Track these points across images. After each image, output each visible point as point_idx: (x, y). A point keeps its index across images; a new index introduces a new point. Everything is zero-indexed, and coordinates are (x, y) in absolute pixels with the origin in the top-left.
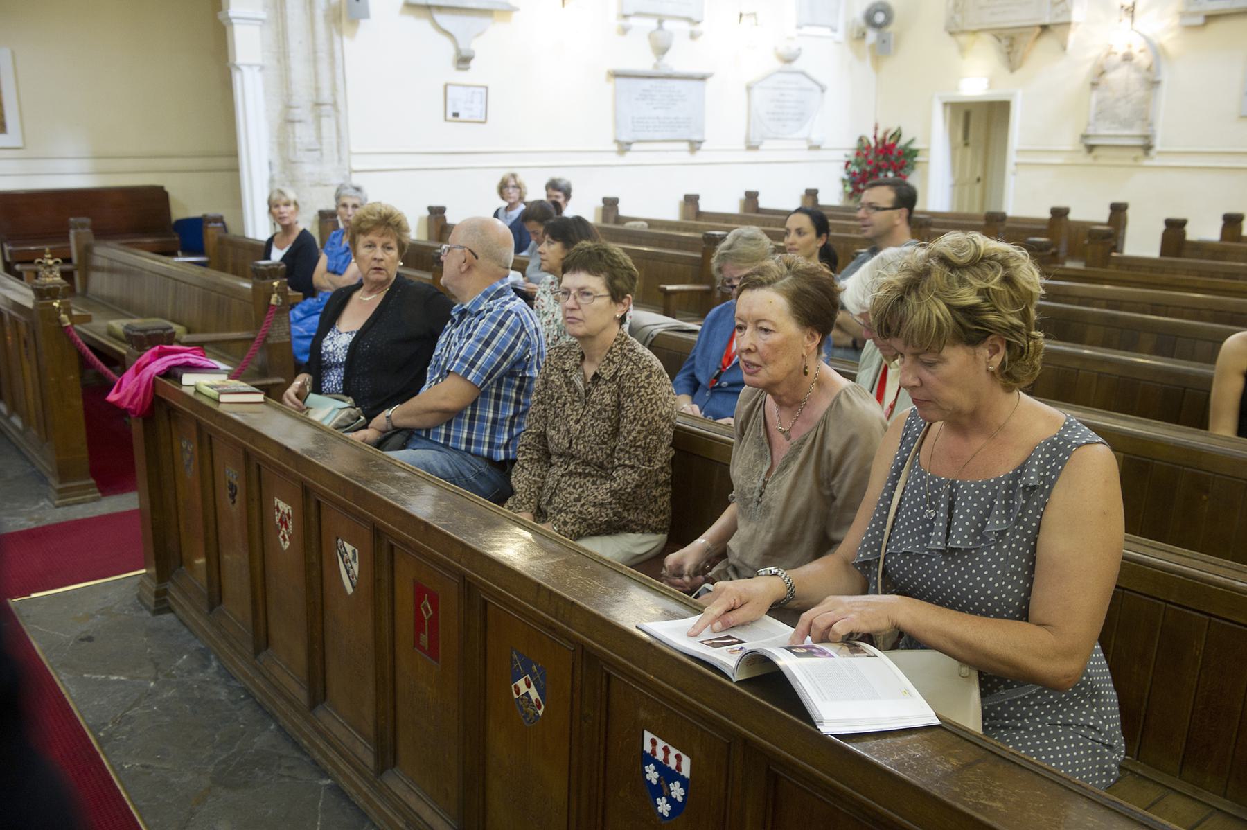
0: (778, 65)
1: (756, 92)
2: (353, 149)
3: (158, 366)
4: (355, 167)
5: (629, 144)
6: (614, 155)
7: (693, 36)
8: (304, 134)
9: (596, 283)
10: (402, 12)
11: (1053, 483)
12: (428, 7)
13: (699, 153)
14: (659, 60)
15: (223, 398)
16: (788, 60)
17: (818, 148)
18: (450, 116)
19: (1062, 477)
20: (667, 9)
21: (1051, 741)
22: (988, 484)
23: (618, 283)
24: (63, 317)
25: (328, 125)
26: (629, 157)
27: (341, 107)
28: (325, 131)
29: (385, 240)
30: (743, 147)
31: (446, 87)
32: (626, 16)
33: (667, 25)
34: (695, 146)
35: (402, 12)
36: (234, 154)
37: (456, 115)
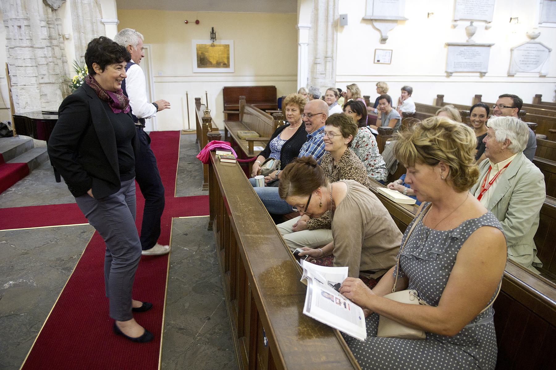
0: (528, 40)
1: (515, 52)
2: (337, 74)
3: (211, 147)
4: (337, 80)
5: (452, 73)
6: (445, 77)
7: (486, 28)
8: (320, 68)
9: (336, 130)
10: (361, 22)
11: (466, 239)
12: (372, 20)
13: (484, 78)
14: (469, 38)
15: (222, 160)
16: (533, 38)
17: (544, 76)
18: (376, 61)
19: (471, 236)
20: (476, 17)
21: (380, 351)
22: (441, 233)
23: (346, 130)
24: (209, 128)
25: (329, 65)
26: (451, 79)
27: (334, 58)
28: (328, 67)
29: (293, 107)
30: (506, 75)
31: (375, 50)
32: (455, 21)
33: (475, 24)
34: (482, 74)
35: (361, 22)
36: (296, 75)
37: (378, 61)
